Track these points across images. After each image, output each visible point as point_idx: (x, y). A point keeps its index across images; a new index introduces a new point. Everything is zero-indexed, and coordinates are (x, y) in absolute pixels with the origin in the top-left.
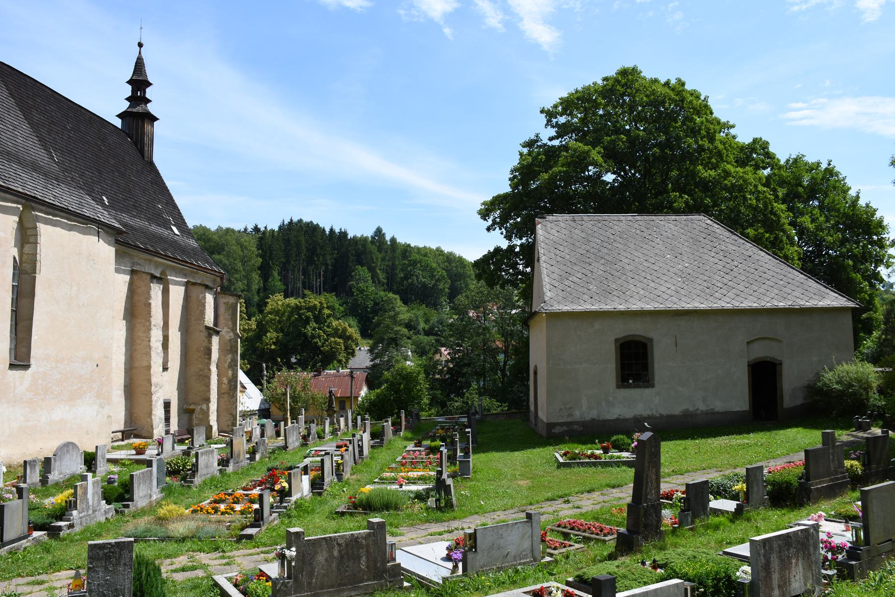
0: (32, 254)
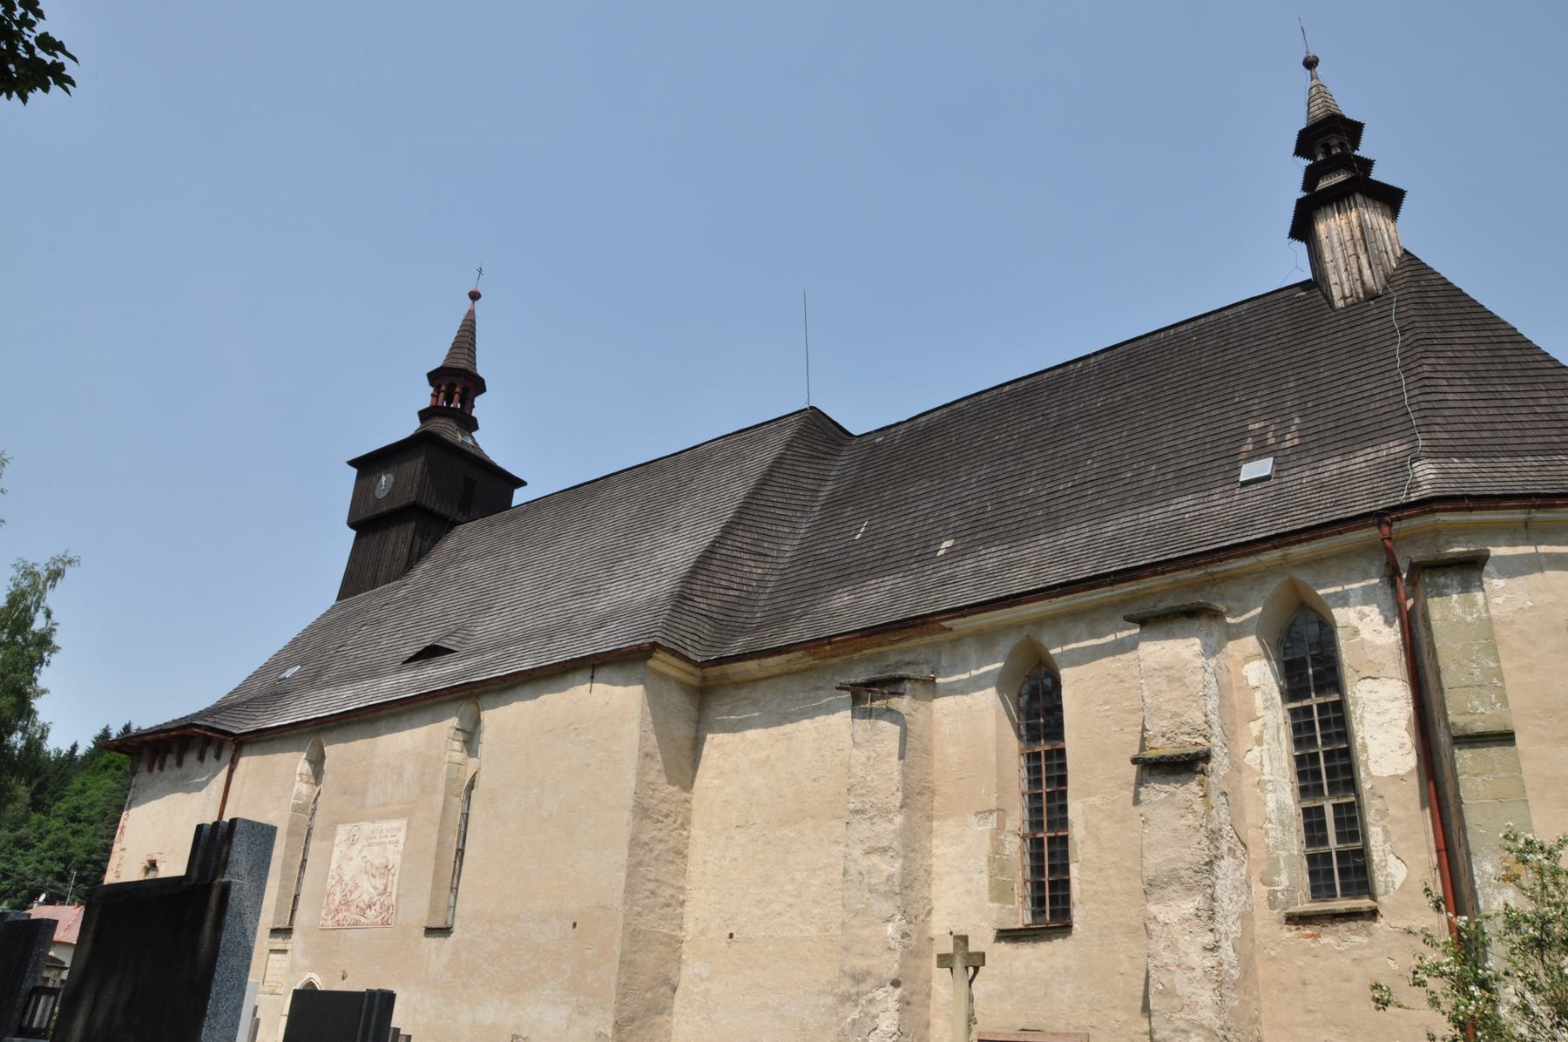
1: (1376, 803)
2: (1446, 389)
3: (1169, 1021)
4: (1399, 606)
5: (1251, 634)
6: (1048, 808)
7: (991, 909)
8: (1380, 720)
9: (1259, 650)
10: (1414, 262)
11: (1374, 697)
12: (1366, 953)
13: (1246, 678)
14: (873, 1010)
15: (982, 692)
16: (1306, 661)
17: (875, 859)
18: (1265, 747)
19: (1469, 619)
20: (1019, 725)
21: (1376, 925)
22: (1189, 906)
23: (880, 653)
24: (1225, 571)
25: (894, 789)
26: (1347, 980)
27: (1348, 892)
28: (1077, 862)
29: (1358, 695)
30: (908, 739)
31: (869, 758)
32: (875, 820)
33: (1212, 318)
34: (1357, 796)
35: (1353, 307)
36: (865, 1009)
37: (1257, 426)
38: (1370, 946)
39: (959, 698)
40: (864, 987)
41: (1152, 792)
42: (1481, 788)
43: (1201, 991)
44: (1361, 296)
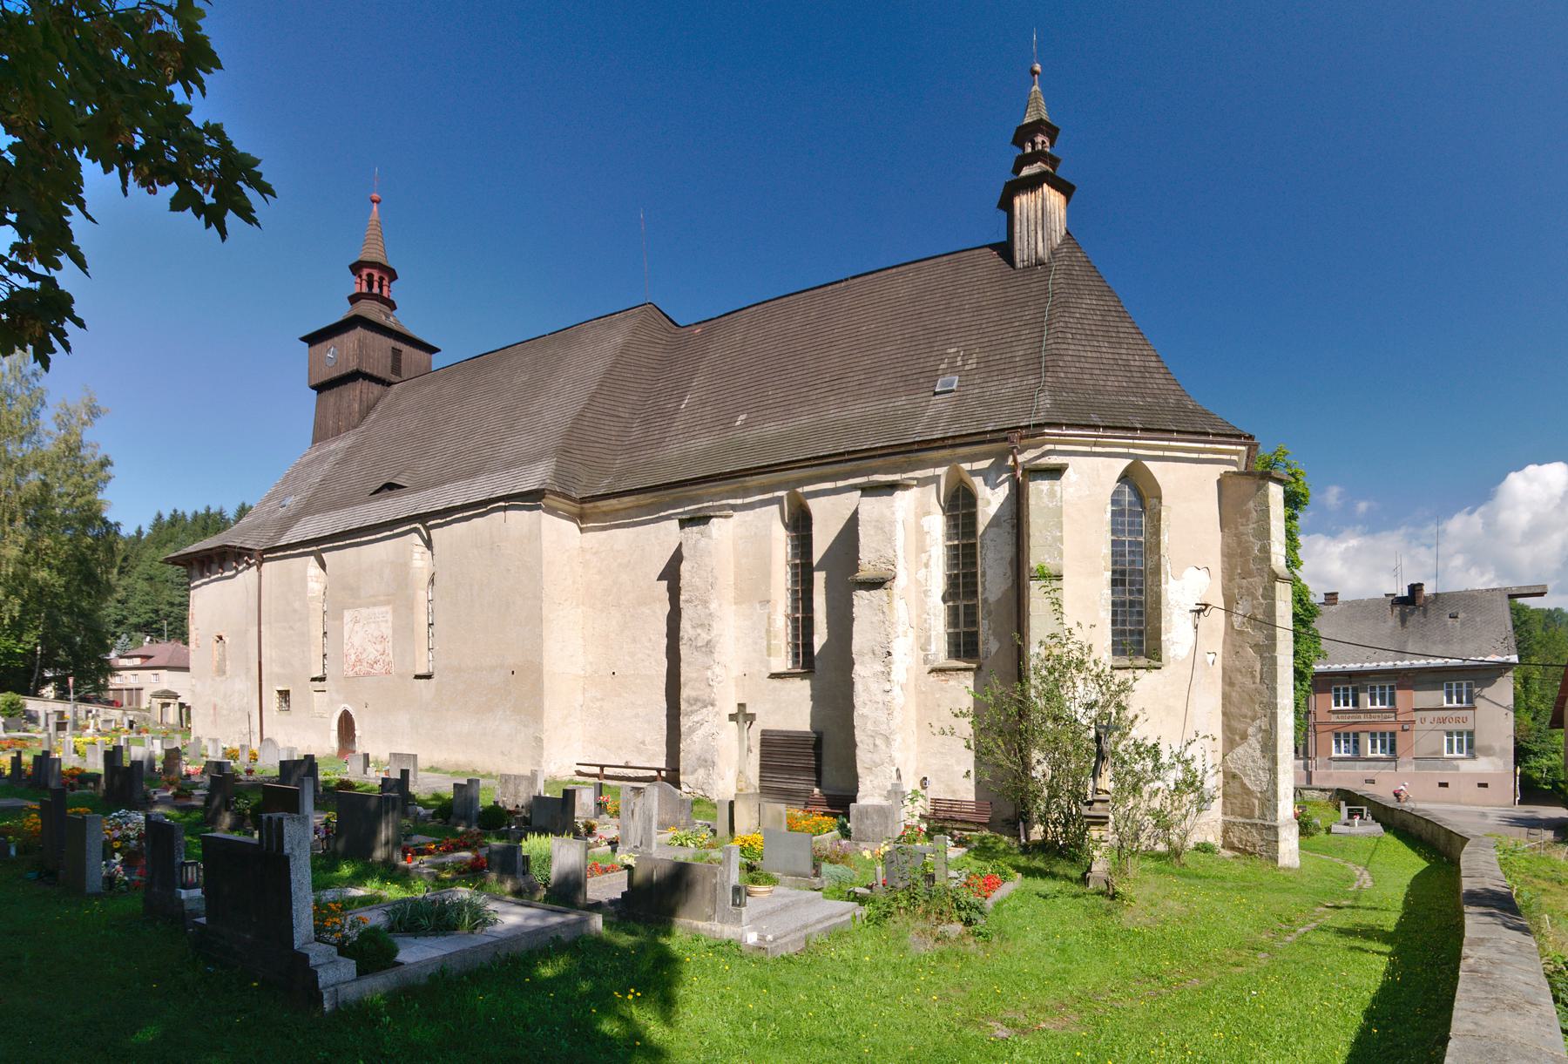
0: (180, 604)
2: (1070, 341)
19: (1050, 505)
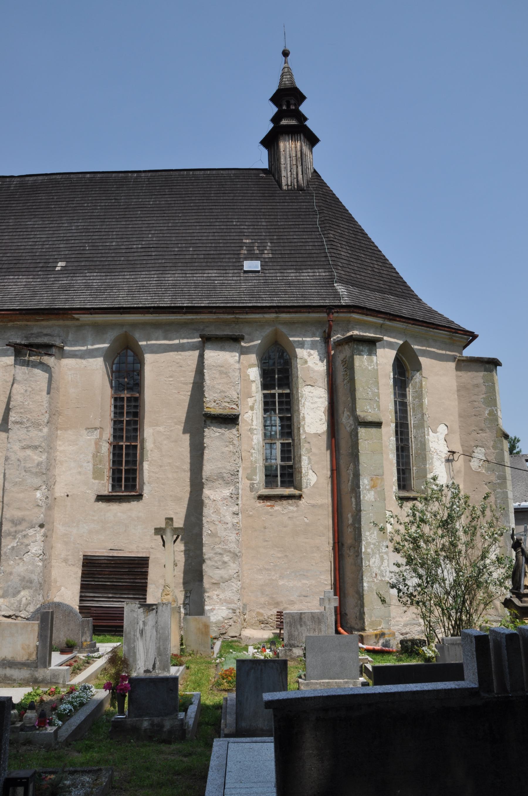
1: (306, 445)
3: (213, 549)
4: (328, 353)
5: (253, 353)
6: (126, 429)
7: (93, 483)
8: (312, 406)
9: (256, 362)
10: (319, 178)
11: (311, 395)
12: (295, 515)
13: (249, 376)
14: (26, 541)
15: (94, 359)
16: (275, 371)
17: (29, 452)
18: (255, 412)
19: (370, 368)
20: (112, 380)
21: (301, 502)
22: (226, 492)
23: (27, 325)
24: (245, 318)
25: (44, 411)
26: (285, 527)
27: (284, 484)
28: (147, 461)
29: (304, 393)
30: (52, 382)
31: (26, 391)
32: (30, 429)
33: (214, 172)
34: (293, 440)
35: (291, 192)
36: (21, 541)
37: (248, 241)
38: (297, 511)
39: (79, 360)
40: (19, 528)
41: (212, 432)
42: (367, 446)
43: (231, 534)
44: (296, 187)
